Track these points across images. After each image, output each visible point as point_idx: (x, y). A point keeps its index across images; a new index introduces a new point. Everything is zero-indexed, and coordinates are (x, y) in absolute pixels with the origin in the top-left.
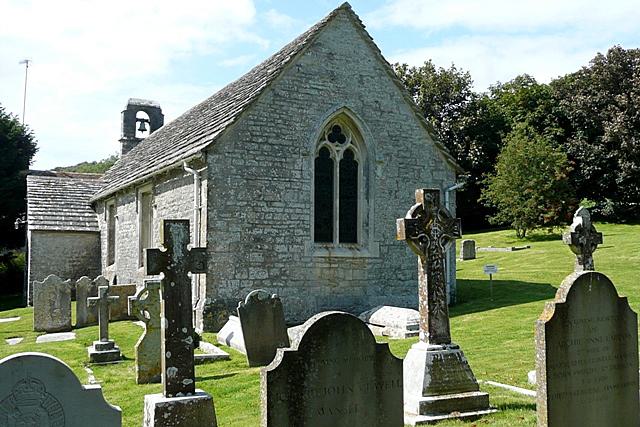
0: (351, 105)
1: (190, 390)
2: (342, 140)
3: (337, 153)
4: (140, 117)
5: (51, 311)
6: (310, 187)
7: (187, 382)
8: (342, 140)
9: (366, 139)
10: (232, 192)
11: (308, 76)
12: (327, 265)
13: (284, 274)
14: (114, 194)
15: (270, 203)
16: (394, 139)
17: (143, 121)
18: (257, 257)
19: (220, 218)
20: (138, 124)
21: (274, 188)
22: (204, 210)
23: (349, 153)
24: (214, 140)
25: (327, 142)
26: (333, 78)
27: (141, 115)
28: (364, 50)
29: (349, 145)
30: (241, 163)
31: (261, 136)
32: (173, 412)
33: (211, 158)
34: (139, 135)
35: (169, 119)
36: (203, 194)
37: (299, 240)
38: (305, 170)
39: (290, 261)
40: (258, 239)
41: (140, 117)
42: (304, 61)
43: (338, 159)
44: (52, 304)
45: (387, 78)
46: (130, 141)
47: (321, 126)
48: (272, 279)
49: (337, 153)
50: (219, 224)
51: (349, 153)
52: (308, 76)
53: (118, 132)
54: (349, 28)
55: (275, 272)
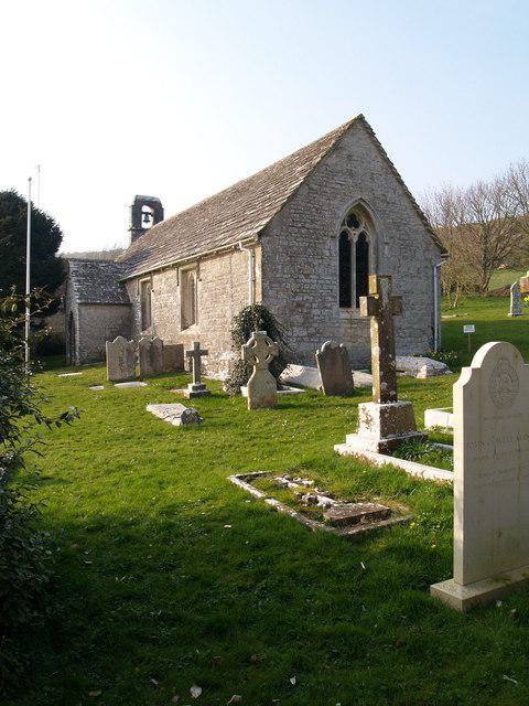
0: (365, 197)
1: (394, 399)
2: (357, 225)
3: (354, 235)
4: (145, 209)
5: (121, 365)
6: (336, 263)
7: (392, 393)
8: (357, 225)
9: (377, 225)
10: (279, 267)
11: (334, 173)
12: (349, 326)
13: (318, 332)
14: (150, 273)
15: (307, 276)
16: (397, 225)
17: (147, 214)
18: (298, 318)
19: (271, 288)
20: (143, 216)
21: (309, 264)
22: (259, 281)
23: (362, 236)
24: (267, 226)
25: (346, 227)
26: (351, 174)
27: (146, 209)
28: (374, 153)
29: (362, 229)
30: (286, 243)
31: (300, 222)
32: (390, 413)
33: (264, 239)
34: (144, 225)
35: (167, 215)
36: (257, 269)
37: (329, 305)
38: (332, 248)
39: (323, 321)
40: (299, 305)
41: (145, 209)
42: (332, 161)
43: (355, 241)
44: (121, 360)
45: (391, 176)
46: (137, 231)
47: (343, 213)
48: (310, 336)
49: (354, 235)
50: (271, 293)
51: (362, 236)
52: (334, 173)
53: (127, 222)
54: (362, 134)
55: (311, 330)
